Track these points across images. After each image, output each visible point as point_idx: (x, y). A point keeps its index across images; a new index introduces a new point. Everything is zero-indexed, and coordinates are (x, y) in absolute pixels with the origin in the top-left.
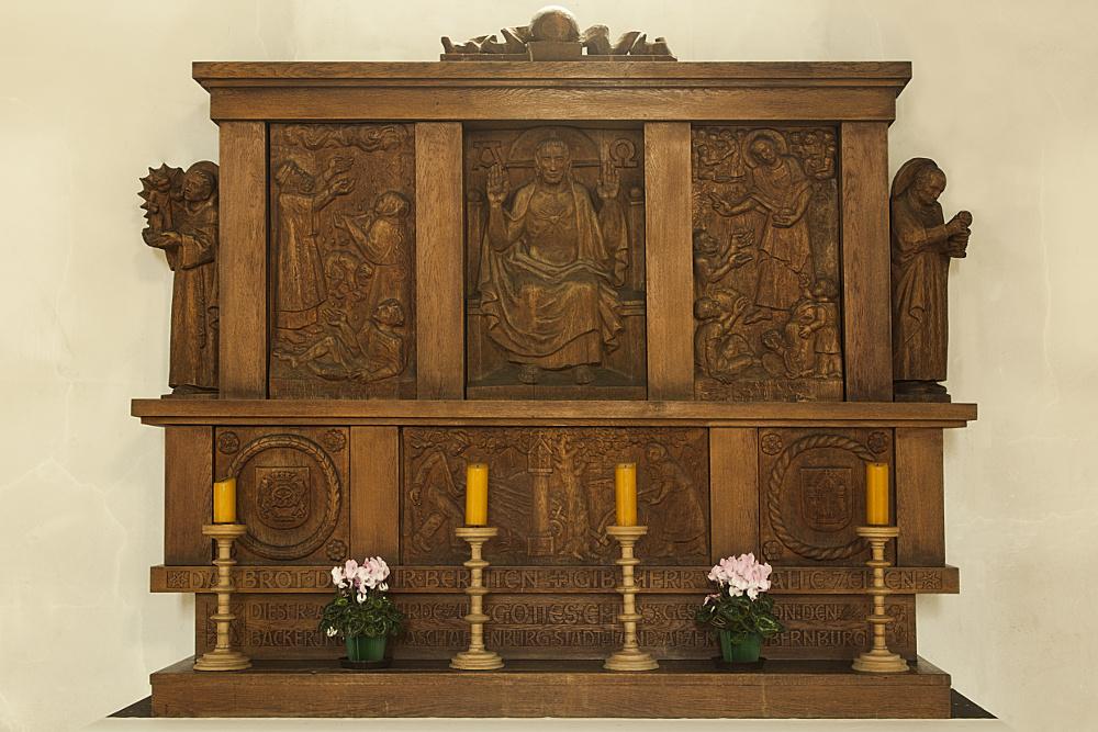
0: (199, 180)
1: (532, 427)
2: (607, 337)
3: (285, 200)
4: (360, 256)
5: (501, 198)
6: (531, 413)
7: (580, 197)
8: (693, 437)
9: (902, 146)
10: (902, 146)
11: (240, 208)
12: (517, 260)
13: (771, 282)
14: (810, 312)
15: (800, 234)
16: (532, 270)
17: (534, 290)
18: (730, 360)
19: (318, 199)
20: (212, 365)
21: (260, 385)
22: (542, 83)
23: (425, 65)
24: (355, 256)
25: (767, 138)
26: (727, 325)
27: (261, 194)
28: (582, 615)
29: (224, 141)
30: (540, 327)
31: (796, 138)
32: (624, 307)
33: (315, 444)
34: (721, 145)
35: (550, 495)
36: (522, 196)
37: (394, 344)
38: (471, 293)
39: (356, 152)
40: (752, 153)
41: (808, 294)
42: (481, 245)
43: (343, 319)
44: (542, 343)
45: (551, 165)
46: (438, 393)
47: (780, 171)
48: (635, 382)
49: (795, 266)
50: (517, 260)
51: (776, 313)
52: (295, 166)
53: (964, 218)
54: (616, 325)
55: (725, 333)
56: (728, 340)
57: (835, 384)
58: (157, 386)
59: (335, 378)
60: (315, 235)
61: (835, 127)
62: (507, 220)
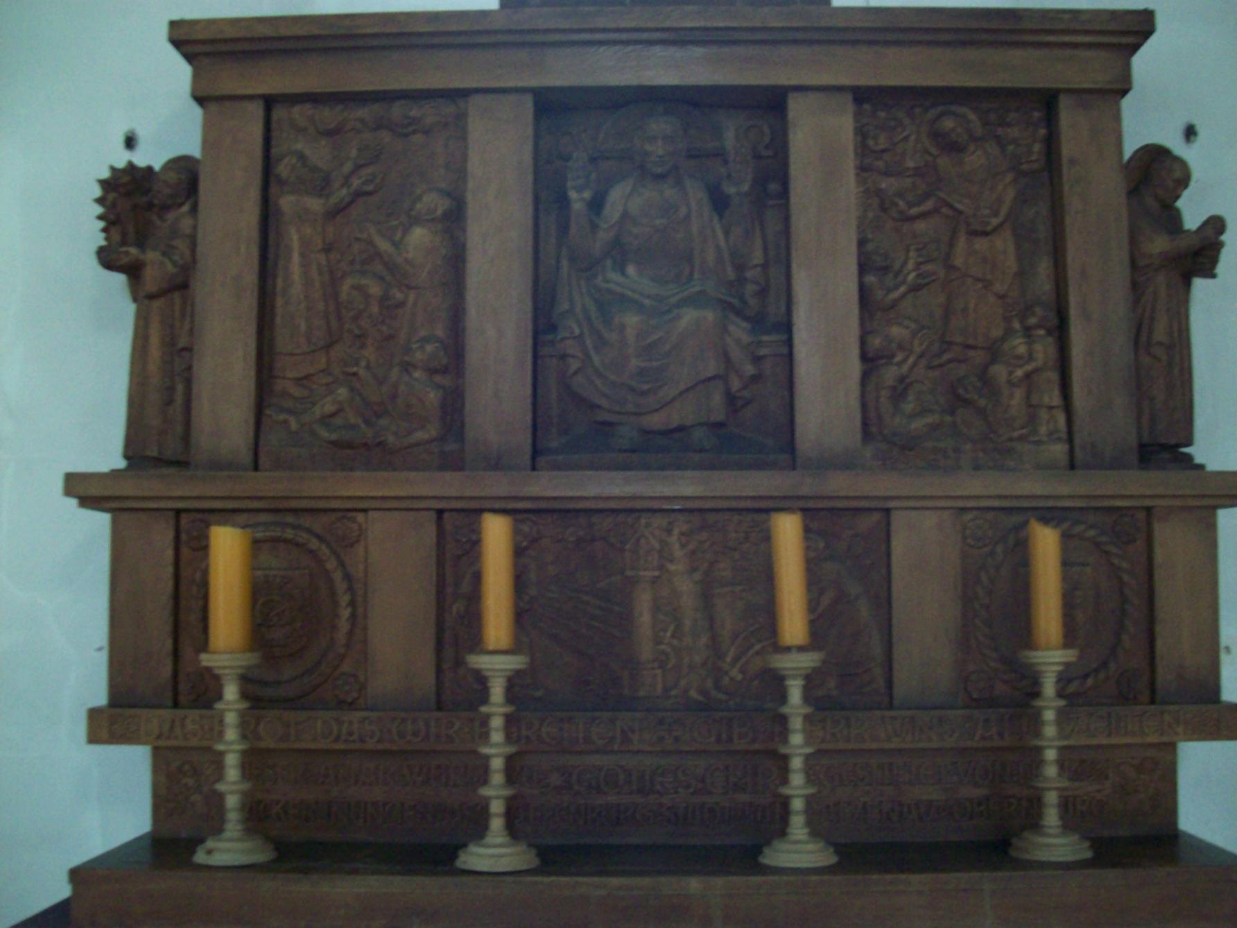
0: (172, 177)
1: (631, 511)
2: (736, 384)
3: (287, 203)
4: (388, 278)
5: (587, 195)
6: (629, 490)
7: (696, 194)
8: (866, 523)
9: (1143, 123)
10: (1143, 123)
11: (224, 230)
12: (607, 281)
13: (965, 310)
14: (1022, 350)
15: (1004, 244)
16: (629, 293)
17: (632, 320)
18: (913, 416)
19: (333, 200)
20: (179, 429)
21: (246, 457)
22: (645, 36)
23: (483, 14)
24: (382, 278)
25: (955, 115)
26: (905, 368)
27: (254, 193)
28: (703, 781)
29: (207, 126)
30: (642, 373)
31: (993, 117)
32: (760, 343)
33: (318, 537)
34: (893, 123)
35: (656, 609)
36: (616, 195)
37: (433, 396)
38: (544, 324)
39: (386, 137)
40: (936, 135)
41: (1016, 325)
42: (558, 261)
43: (363, 363)
44: (643, 394)
45: (658, 149)
46: (496, 463)
47: (975, 159)
48: (781, 444)
49: (999, 288)
50: (607, 281)
51: (971, 353)
52: (302, 157)
53: (1216, 225)
54: (749, 369)
55: (902, 379)
56: (906, 389)
57: (1059, 450)
58: (105, 454)
59: (350, 445)
60: (327, 249)
61: (1048, 101)
62: (594, 227)
